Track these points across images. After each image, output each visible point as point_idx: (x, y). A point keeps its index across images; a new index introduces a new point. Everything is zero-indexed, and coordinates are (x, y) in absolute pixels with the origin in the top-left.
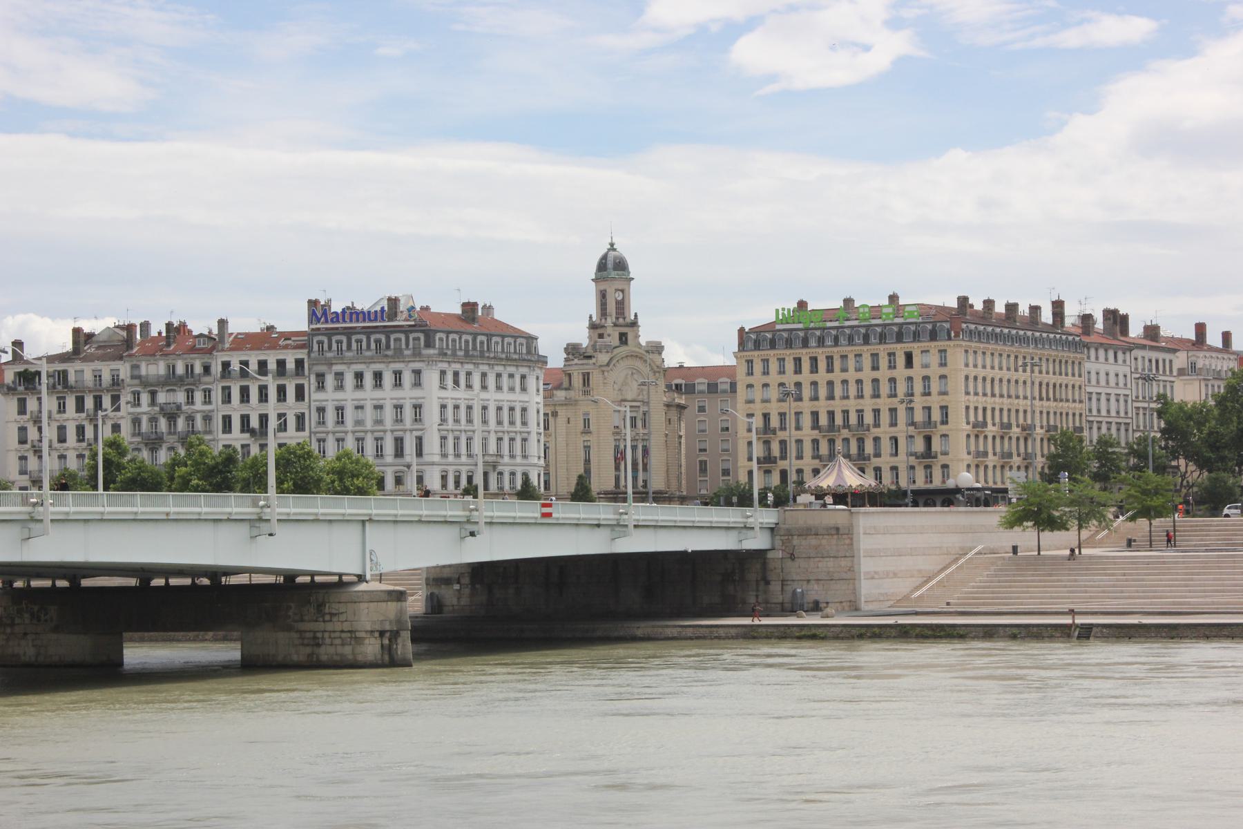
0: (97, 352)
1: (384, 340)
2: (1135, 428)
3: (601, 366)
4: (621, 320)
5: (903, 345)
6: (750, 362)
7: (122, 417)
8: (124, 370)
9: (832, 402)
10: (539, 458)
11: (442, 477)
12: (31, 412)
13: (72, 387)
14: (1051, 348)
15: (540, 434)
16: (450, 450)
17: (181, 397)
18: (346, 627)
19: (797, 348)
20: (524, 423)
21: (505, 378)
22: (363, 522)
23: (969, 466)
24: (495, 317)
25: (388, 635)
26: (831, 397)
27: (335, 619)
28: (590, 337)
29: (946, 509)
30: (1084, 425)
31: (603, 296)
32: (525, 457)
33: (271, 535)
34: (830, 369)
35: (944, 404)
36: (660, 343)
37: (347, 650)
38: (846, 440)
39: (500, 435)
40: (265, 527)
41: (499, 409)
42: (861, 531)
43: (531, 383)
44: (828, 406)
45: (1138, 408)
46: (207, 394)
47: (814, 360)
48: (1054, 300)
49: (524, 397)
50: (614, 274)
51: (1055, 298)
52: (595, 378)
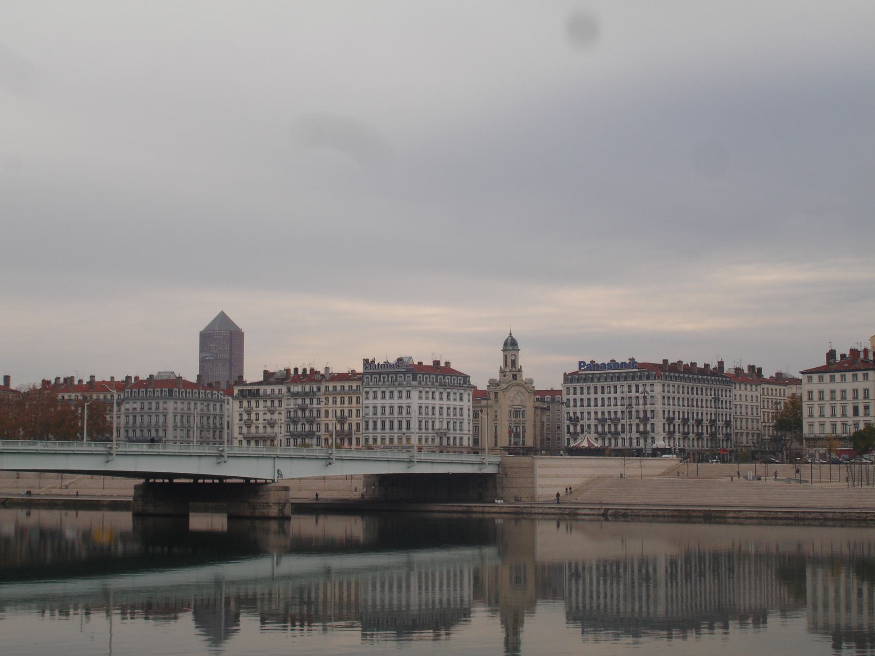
0: (668, 366)
1: (395, 377)
2: (762, 421)
3: (503, 390)
4: (514, 369)
5: (635, 382)
6: (568, 388)
7: (282, 410)
8: (284, 389)
9: (604, 407)
10: (469, 431)
11: (419, 439)
12: (244, 407)
13: (262, 396)
14: (713, 383)
15: (470, 420)
16: (423, 426)
17: (300, 401)
18: (265, 501)
19: (652, 380)
20: (461, 415)
21: (452, 395)
22: (275, 458)
23: (664, 438)
24: (451, 367)
25: (282, 505)
26: (603, 405)
27: (261, 498)
28: (500, 376)
29: (653, 458)
30: (732, 420)
31: (506, 357)
32: (461, 430)
33: (225, 462)
34: (603, 392)
35: (652, 409)
36: (532, 379)
37: (265, 511)
38: (609, 425)
39: (449, 420)
40: (222, 459)
41: (449, 408)
42: (538, 466)
43: (465, 397)
44: (602, 409)
45: (764, 412)
46: (319, 399)
47: (596, 388)
48: (719, 361)
49: (461, 403)
50: (511, 348)
51: (720, 360)
52: (500, 395)
